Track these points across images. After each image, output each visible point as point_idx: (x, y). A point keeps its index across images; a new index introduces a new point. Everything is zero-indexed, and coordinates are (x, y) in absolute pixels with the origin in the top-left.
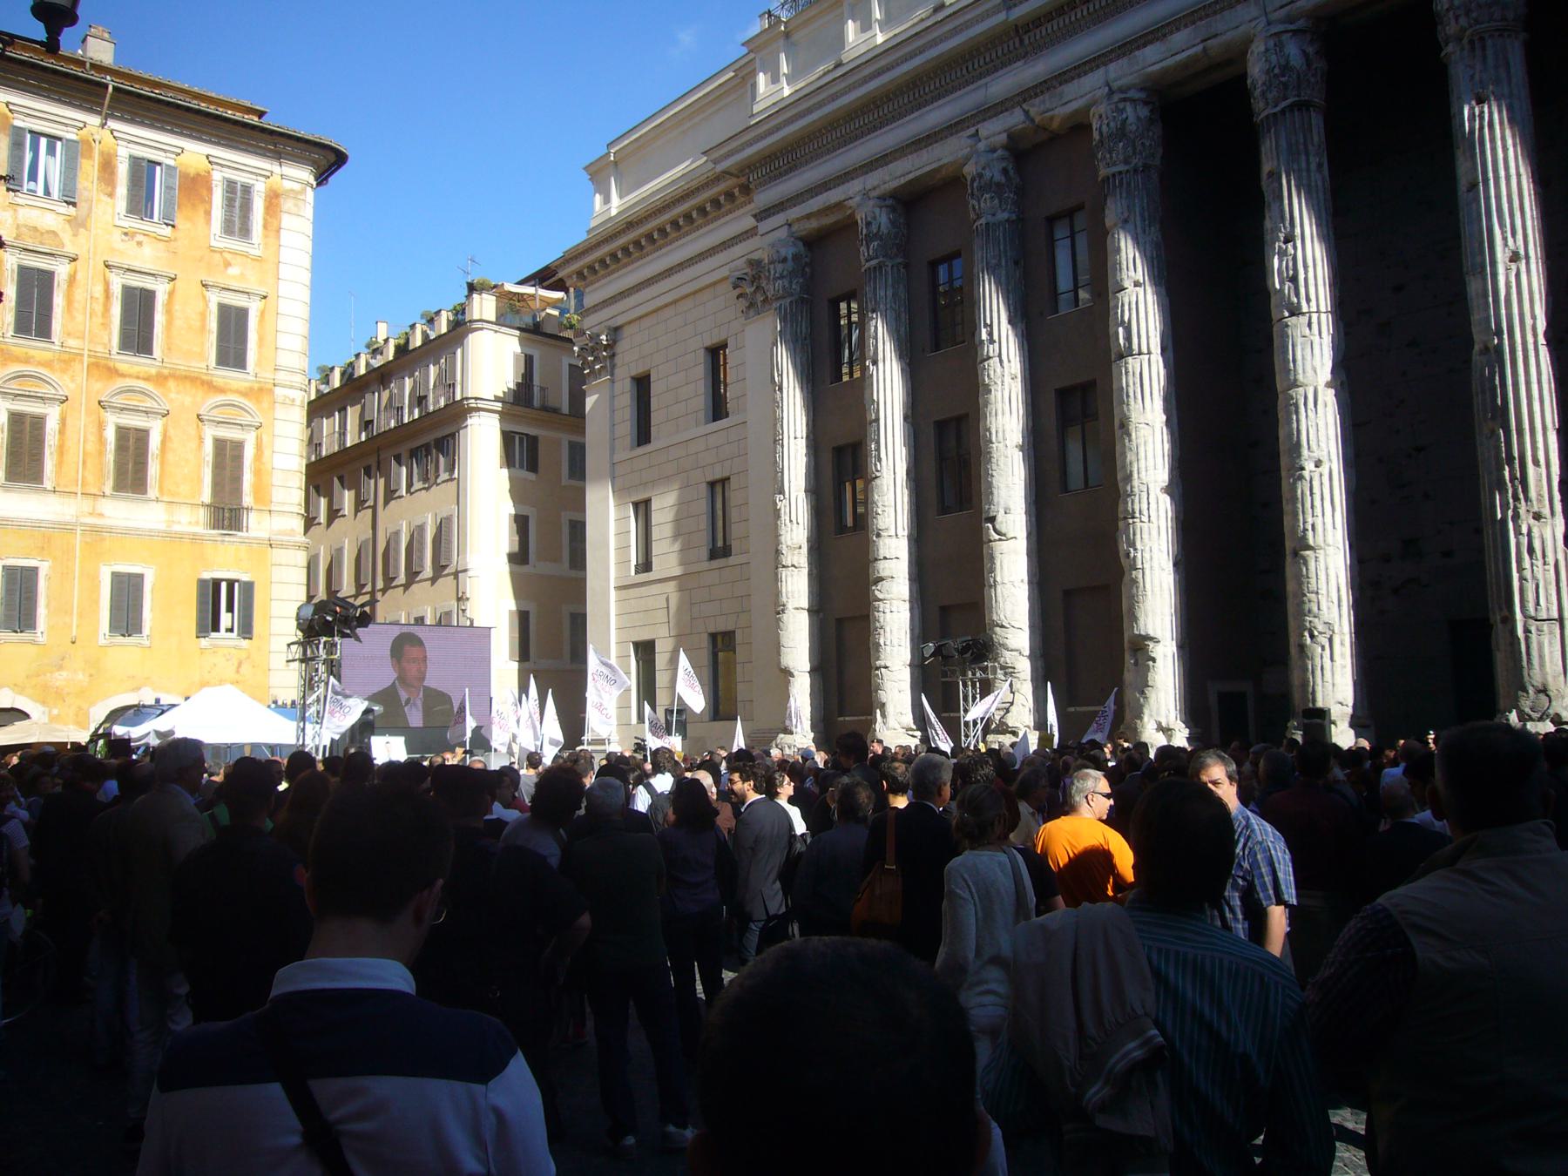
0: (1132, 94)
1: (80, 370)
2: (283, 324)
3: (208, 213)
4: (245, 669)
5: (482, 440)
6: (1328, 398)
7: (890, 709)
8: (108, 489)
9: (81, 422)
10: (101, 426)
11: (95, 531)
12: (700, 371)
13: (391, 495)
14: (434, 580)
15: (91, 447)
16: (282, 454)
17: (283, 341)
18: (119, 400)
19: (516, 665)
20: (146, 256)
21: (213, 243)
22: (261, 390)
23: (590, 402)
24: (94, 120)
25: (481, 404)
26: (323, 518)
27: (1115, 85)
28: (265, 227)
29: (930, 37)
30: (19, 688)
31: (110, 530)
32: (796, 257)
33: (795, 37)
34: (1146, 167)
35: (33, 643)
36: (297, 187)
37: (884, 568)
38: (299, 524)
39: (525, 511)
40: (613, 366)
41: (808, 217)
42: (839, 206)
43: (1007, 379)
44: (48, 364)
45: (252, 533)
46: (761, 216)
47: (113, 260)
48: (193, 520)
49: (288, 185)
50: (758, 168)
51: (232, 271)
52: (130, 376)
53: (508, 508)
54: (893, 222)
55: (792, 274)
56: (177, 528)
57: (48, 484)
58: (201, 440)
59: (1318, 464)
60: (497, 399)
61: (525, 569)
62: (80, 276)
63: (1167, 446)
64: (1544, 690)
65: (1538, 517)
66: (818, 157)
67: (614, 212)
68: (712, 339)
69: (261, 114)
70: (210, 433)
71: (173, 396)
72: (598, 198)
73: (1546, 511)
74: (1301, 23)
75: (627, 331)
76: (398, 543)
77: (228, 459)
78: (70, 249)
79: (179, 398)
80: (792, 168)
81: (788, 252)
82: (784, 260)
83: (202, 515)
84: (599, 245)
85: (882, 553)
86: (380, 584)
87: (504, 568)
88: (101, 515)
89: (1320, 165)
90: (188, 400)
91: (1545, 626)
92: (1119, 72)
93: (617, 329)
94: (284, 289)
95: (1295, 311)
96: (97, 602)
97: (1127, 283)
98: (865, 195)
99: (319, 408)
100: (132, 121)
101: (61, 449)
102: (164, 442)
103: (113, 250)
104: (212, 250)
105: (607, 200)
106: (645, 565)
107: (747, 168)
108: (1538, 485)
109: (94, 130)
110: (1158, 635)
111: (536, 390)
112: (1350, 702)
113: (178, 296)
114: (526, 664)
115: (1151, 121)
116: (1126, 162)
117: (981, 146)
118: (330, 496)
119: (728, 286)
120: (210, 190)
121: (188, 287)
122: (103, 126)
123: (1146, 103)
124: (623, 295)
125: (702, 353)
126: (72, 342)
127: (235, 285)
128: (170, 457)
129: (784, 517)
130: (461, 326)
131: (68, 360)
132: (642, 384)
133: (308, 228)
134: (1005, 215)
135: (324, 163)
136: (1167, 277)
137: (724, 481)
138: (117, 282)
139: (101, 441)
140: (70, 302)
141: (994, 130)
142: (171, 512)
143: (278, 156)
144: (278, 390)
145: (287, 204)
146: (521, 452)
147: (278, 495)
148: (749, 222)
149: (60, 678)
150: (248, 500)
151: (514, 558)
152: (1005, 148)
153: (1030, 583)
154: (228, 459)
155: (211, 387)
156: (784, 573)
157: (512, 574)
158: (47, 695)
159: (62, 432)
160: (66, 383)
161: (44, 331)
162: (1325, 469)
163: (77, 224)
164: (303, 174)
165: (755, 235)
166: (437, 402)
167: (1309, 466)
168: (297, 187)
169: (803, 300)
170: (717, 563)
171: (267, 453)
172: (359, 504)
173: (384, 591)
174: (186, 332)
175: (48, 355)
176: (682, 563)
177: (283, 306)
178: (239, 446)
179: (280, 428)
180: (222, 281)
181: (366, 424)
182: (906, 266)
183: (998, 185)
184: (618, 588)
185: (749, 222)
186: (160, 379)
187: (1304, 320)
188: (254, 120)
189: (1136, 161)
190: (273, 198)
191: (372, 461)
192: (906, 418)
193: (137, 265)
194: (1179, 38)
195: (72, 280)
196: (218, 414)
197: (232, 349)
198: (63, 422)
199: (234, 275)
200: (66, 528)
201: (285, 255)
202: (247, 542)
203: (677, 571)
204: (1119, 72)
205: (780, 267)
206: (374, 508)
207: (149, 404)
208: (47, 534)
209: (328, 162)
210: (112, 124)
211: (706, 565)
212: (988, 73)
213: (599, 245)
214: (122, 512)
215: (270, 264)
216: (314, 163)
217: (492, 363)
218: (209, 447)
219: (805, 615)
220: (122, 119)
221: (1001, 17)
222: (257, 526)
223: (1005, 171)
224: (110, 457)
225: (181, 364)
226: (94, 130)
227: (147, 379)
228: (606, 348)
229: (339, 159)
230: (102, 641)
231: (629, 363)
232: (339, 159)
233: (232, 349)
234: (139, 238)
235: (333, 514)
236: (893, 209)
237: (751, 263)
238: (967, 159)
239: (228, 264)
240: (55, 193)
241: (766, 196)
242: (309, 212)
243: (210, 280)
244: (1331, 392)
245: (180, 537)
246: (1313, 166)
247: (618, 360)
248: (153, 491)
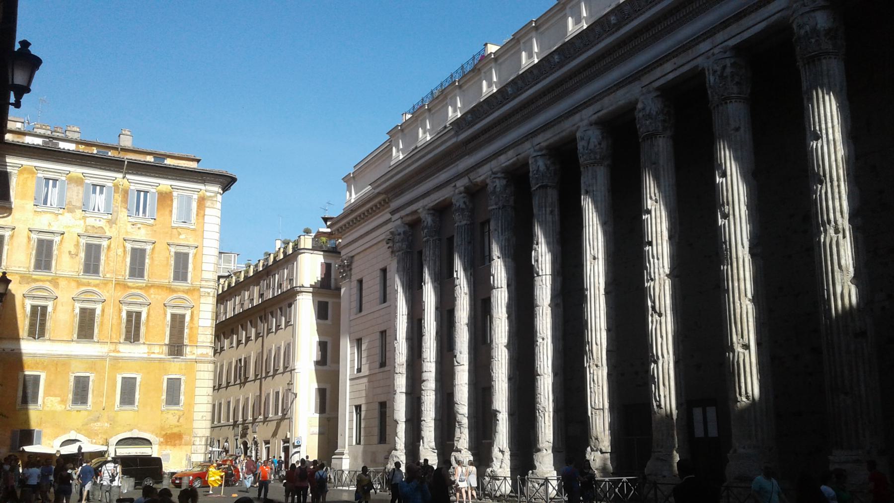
0: (499, 175)
1: (111, 286)
2: (205, 259)
3: (171, 211)
4: (181, 420)
5: (305, 309)
6: (466, 329)
7: (425, 440)
8: (122, 341)
9: (111, 311)
10: (120, 311)
11: (116, 359)
12: (378, 280)
13: (269, 331)
14: (283, 373)
15: (115, 322)
16: (203, 319)
17: (205, 267)
18: (129, 300)
19: (318, 415)
20: (142, 234)
21: (173, 225)
22: (194, 290)
23: (343, 290)
24: (120, 176)
25: (302, 289)
26: (253, 337)
27: (494, 170)
28: (197, 215)
29: (435, 145)
30: (79, 431)
31: (122, 358)
32: (404, 232)
33: (406, 131)
34: (504, 207)
35: (86, 410)
36: (212, 194)
37: (425, 376)
38: (211, 352)
39: (324, 339)
40: (351, 275)
41: (407, 215)
42: (415, 212)
43: (463, 295)
44: (96, 286)
45: (189, 357)
46: (393, 213)
47: (127, 237)
48: (160, 351)
49: (208, 194)
50: (390, 189)
51: (181, 237)
52: (133, 288)
53: (316, 338)
54: (433, 221)
55: (403, 240)
56: (153, 356)
57: (95, 339)
58: (165, 314)
59: (543, 339)
60: (311, 286)
61: (325, 368)
62: (112, 246)
63: (507, 328)
64: (597, 439)
65: (597, 366)
66: (409, 189)
67: (353, 201)
68: (382, 266)
69: (198, 161)
70: (169, 312)
71: (153, 296)
72: (348, 193)
73: (600, 364)
74: (543, 152)
75: (356, 258)
76: (270, 357)
77: (178, 323)
78: (108, 234)
79: (155, 297)
80: (402, 193)
81: (401, 230)
82: (399, 234)
83: (165, 349)
84: (349, 214)
85: (425, 369)
86: (264, 375)
87: (312, 367)
88: (119, 352)
89: (552, 212)
90: (159, 297)
91: (597, 412)
92: (494, 165)
93: (353, 257)
94: (206, 243)
95: (538, 275)
96: (115, 391)
97: (495, 257)
98: (424, 207)
99: (222, 299)
100: (137, 174)
101: (102, 323)
102: (148, 316)
103: (127, 232)
104: (173, 228)
105: (351, 195)
106: (359, 370)
107: (386, 191)
108: (597, 354)
109: (120, 180)
110: (500, 410)
111: (333, 281)
112: (552, 441)
113: (157, 249)
114: (324, 415)
115: (506, 186)
116: (496, 204)
117: (457, 191)
118: (256, 327)
119: (384, 243)
120: (172, 200)
121: (161, 246)
122: (124, 178)
123: (504, 178)
124: (361, 237)
125: (379, 272)
126: (108, 276)
127: (182, 243)
128: (151, 324)
129: (397, 352)
130: (297, 250)
131: (106, 282)
132: (360, 282)
133: (219, 213)
134: (465, 222)
135: (226, 183)
136: (505, 255)
137: (385, 331)
138: (129, 246)
139: (120, 317)
140: (107, 257)
141: (461, 184)
142: (153, 345)
143: (204, 182)
144: (202, 290)
145: (208, 203)
146: (322, 312)
147: (201, 338)
148: (388, 216)
149: (96, 426)
150: (186, 342)
151: (317, 363)
152: (465, 192)
153: (469, 384)
154: (178, 323)
155: (172, 290)
156: (396, 376)
157: (316, 370)
158: (90, 435)
159: (103, 315)
160: (105, 294)
161: (96, 271)
162: (545, 342)
163: (111, 222)
164: (216, 188)
165: (386, 223)
166: (286, 286)
167: (540, 340)
168: (212, 194)
169: (408, 252)
170: (382, 369)
171: (196, 319)
172: (258, 335)
173: (265, 378)
174: (159, 267)
175: (98, 282)
176: (370, 370)
177: (205, 251)
178: (183, 316)
179: (202, 307)
180: (176, 242)
181: (261, 295)
182: (440, 240)
183: (463, 209)
184: (351, 380)
185: (388, 216)
186: (148, 287)
187: (540, 278)
188: (193, 165)
189: (500, 204)
190: (202, 201)
191: (263, 314)
192: (437, 308)
193: (137, 238)
194: (511, 153)
195: (109, 247)
196: (173, 303)
197: (181, 273)
198: (103, 311)
199: (183, 239)
200: (102, 358)
201: (207, 227)
202: (186, 361)
203: (367, 373)
204: (494, 165)
205: (398, 237)
206: (263, 336)
207: (141, 300)
208: (93, 362)
209: (227, 182)
210: (128, 176)
211: (377, 371)
212: (458, 160)
213: (349, 214)
214: (128, 350)
215: (199, 232)
216: (221, 183)
217: (310, 268)
218: (169, 318)
219: (404, 395)
220: (132, 174)
221: (454, 140)
222: (190, 352)
223: (465, 203)
224: (124, 325)
225: (156, 280)
226: (120, 180)
227: (141, 288)
228: (348, 266)
229: (233, 180)
230: (116, 409)
231: (356, 275)
232: (233, 180)
233: (181, 273)
234: (139, 226)
235: (248, 339)
236: (434, 215)
237: (392, 233)
238: (453, 195)
239: (180, 234)
240: (102, 211)
241: (394, 205)
242: (219, 206)
243: (171, 242)
244: (549, 309)
245: (154, 360)
246: (548, 212)
247: (353, 272)
248: (141, 341)
